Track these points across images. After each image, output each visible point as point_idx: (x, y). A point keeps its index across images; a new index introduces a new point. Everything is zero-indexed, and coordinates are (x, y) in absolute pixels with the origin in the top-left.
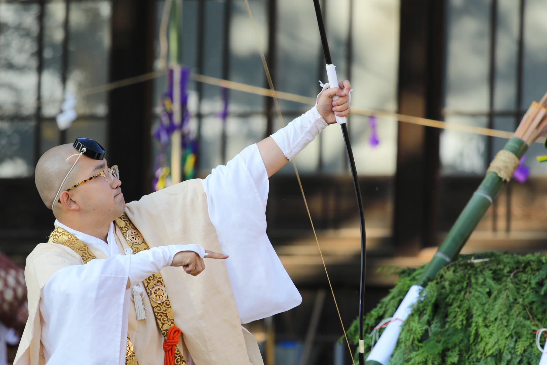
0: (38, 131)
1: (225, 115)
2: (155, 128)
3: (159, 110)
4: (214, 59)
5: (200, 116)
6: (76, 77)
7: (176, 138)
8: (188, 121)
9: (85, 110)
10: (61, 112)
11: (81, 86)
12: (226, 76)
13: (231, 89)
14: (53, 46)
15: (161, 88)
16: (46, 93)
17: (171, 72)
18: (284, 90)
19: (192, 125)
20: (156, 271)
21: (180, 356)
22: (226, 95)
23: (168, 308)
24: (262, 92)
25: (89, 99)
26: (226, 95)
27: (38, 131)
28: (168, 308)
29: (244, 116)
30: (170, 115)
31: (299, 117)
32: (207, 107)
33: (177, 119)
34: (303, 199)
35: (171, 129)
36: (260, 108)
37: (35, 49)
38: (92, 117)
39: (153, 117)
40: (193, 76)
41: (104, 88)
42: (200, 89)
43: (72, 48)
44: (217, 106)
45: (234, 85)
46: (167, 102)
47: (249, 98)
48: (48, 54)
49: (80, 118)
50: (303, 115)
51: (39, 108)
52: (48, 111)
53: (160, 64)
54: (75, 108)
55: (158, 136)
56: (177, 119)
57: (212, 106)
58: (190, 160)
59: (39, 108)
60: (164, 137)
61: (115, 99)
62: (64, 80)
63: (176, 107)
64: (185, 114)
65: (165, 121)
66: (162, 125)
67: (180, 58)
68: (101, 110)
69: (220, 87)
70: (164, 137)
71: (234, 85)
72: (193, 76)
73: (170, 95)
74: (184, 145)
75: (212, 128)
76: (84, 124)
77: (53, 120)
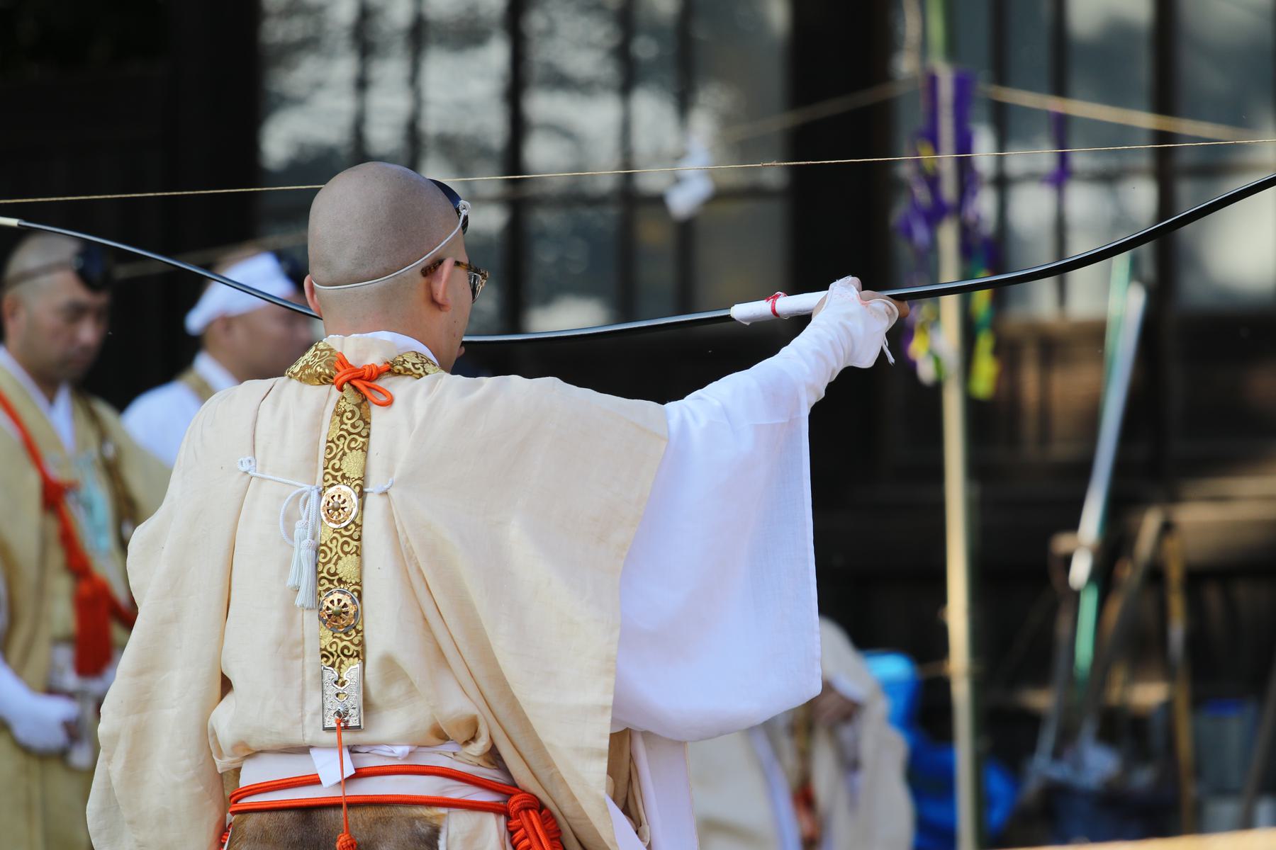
0: (626, 229)
1: (1061, 176)
2: (899, 212)
4: (1031, 50)
5: (1002, 183)
7: (948, 237)
8: (974, 194)
9: (734, 173)
10: (678, 181)
11: (726, 121)
12: (1060, 88)
14: (656, 31)
15: (910, 119)
16: (643, 142)
17: (932, 81)
18: (1196, 116)
19: (985, 204)
21: (342, 423)
22: (1061, 129)
23: (332, 441)
24: (1145, 120)
25: (743, 149)
26: (1061, 129)
27: (626, 229)
28: (332, 441)
29: (1109, 178)
30: (933, 181)
31: (651, 405)
32: (1017, 161)
33: (949, 190)
34: (936, 473)
35: (935, 214)
37: (612, 42)
38: (755, 193)
40: (985, 89)
41: (779, 122)
43: (701, 32)
44: (1043, 157)
45: (1079, 108)
46: (926, 156)
47: (1122, 133)
49: (720, 196)
50: (784, 350)
52: (650, 179)
53: (906, 65)
54: (710, 173)
55: (908, 232)
56: (949, 190)
57: (1037, 156)
59: (628, 178)
60: (920, 233)
62: (684, 104)
63: (946, 161)
64: (966, 173)
65: (922, 195)
66: (915, 205)
67: (953, 50)
68: (772, 172)
69: (1048, 112)
70: (920, 233)
71: (1079, 108)
72: (985, 89)
73: (932, 138)
74: (968, 249)
75: (1031, 209)
76: (734, 209)
77: (658, 201)
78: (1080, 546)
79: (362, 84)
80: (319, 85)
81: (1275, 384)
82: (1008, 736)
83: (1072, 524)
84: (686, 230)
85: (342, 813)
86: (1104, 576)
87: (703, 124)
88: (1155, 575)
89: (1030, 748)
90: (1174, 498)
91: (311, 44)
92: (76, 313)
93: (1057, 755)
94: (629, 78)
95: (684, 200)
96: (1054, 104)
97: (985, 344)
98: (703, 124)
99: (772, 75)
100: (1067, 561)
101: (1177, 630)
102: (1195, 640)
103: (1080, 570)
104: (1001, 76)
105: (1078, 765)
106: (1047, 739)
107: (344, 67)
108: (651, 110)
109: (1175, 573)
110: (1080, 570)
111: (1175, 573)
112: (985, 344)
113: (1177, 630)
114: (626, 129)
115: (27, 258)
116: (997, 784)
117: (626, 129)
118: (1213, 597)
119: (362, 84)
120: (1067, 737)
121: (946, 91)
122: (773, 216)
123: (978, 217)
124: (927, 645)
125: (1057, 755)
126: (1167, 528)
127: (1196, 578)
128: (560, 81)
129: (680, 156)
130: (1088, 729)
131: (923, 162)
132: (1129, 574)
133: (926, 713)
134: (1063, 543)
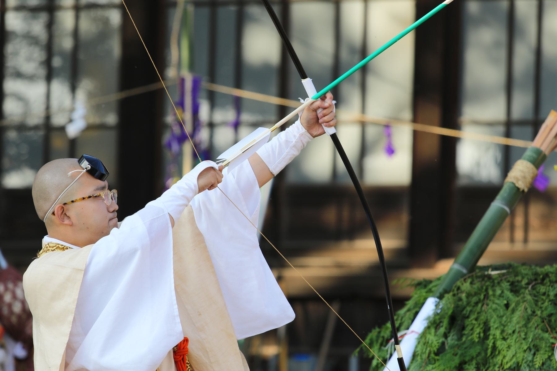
3: (169, 119)
6: (86, 85)
8: (199, 130)
11: (91, 95)
15: (171, 99)
17: (182, 81)
19: (203, 135)
30: (181, 125)
33: (188, 129)
35: (182, 139)
38: (102, 127)
41: (114, 97)
42: (212, 97)
48: (57, 62)
49: (89, 128)
51: (48, 118)
52: (58, 120)
53: (171, 73)
54: (85, 117)
56: (188, 129)
58: (330, 215)
59: (48, 118)
61: (125, 109)
62: (73, 89)
63: (188, 116)
65: (177, 130)
68: (111, 119)
70: (175, 147)
71: (246, 94)
73: (181, 104)
77: (62, 129)
95: (73, 130)
108: (60, 89)
121: (189, 85)
131: (175, 117)
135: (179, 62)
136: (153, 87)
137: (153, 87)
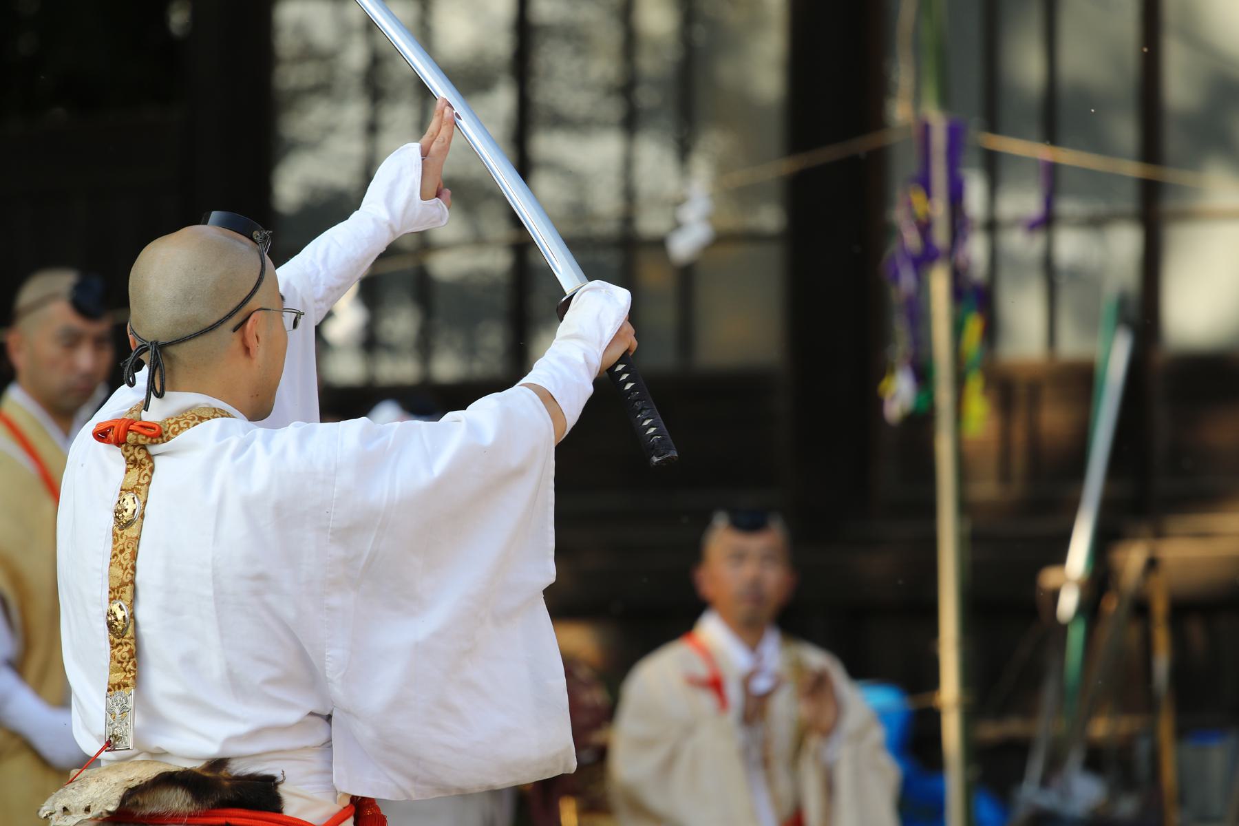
1: (1047, 222)
3: (899, 216)
6: (713, 145)
7: (939, 283)
8: (964, 238)
9: (732, 221)
10: (678, 226)
11: (722, 168)
13: (902, 237)
15: (904, 165)
17: (926, 130)
19: (976, 249)
20: (280, 779)
25: (742, 196)
29: (1096, 223)
30: (925, 228)
33: (941, 236)
34: (929, 510)
35: (925, 259)
36: (1128, 201)
38: (753, 237)
39: (887, 231)
41: (777, 168)
42: (993, 165)
46: (918, 199)
48: (647, 97)
49: (721, 239)
51: (628, 219)
52: (650, 223)
53: (900, 111)
54: (709, 219)
56: (941, 236)
58: (974, 327)
59: (628, 219)
61: (800, 194)
62: (684, 151)
63: (939, 209)
64: (958, 222)
65: (912, 239)
68: (769, 218)
69: (1036, 161)
70: (907, 280)
71: (1065, 156)
73: (925, 183)
77: (659, 244)
78: (1067, 580)
79: (372, 129)
80: (330, 130)
81: (1233, 430)
82: (996, 767)
83: (1058, 555)
84: (687, 274)
85: (1132, 169)
86: (1090, 608)
87: (702, 172)
88: (1140, 608)
89: (1018, 776)
90: (1159, 534)
91: (324, 89)
92: (72, 341)
93: (1045, 782)
94: (631, 123)
95: (684, 245)
96: (1043, 152)
97: (975, 386)
98: (702, 172)
99: (773, 132)
100: (1055, 595)
101: (1162, 663)
102: (1179, 671)
103: (1068, 603)
104: (993, 124)
105: (1066, 794)
106: (1036, 767)
107: (354, 112)
108: (654, 159)
109: (1160, 607)
110: (1068, 603)
111: (1160, 607)
112: (975, 386)
113: (1162, 663)
114: (628, 165)
115: (31, 292)
116: (987, 811)
117: (628, 165)
118: (1196, 631)
119: (372, 129)
120: (1055, 764)
121: (939, 139)
122: (770, 261)
123: (968, 262)
124: (918, 677)
125: (1045, 782)
126: (1152, 564)
127: (1185, 609)
128: (560, 121)
129: (679, 202)
130: (1075, 759)
131: (912, 211)
132: (1111, 605)
133: (917, 743)
134: (1050, 577)
135: (913, 106)
136: (861, 146)
137: (861, 146)
